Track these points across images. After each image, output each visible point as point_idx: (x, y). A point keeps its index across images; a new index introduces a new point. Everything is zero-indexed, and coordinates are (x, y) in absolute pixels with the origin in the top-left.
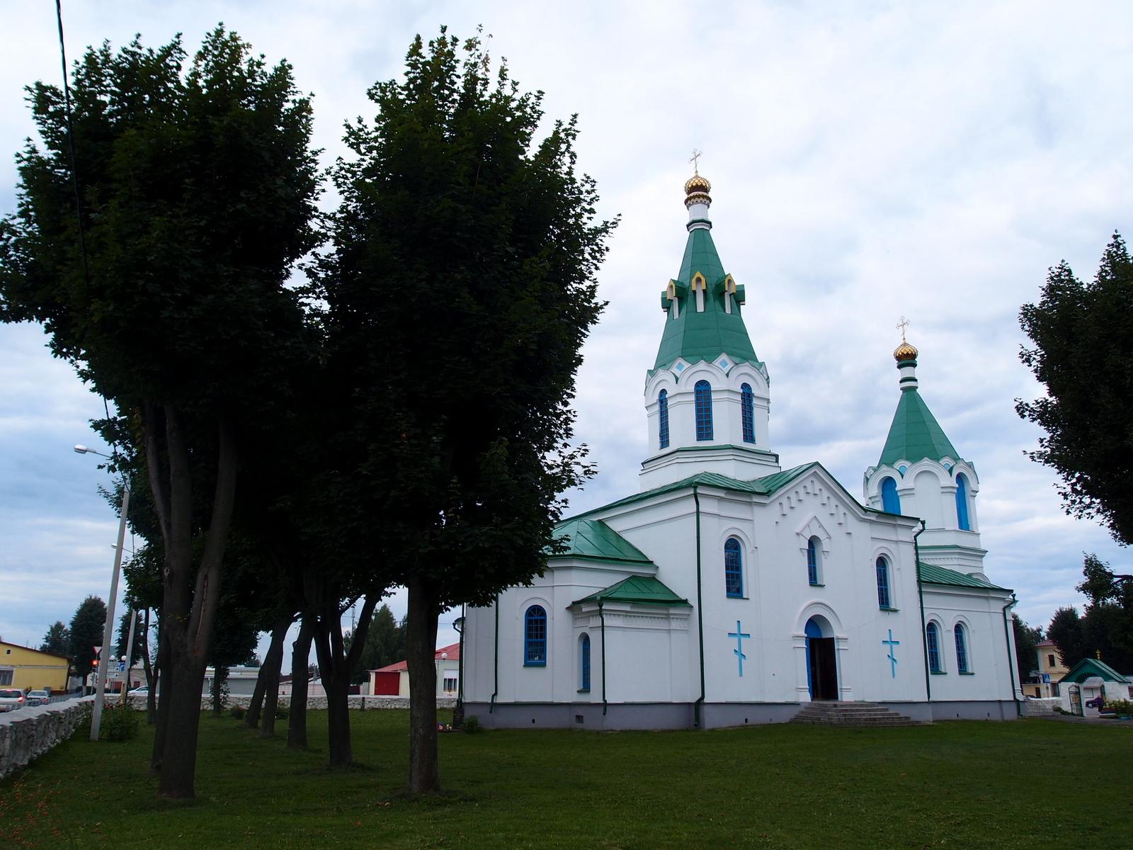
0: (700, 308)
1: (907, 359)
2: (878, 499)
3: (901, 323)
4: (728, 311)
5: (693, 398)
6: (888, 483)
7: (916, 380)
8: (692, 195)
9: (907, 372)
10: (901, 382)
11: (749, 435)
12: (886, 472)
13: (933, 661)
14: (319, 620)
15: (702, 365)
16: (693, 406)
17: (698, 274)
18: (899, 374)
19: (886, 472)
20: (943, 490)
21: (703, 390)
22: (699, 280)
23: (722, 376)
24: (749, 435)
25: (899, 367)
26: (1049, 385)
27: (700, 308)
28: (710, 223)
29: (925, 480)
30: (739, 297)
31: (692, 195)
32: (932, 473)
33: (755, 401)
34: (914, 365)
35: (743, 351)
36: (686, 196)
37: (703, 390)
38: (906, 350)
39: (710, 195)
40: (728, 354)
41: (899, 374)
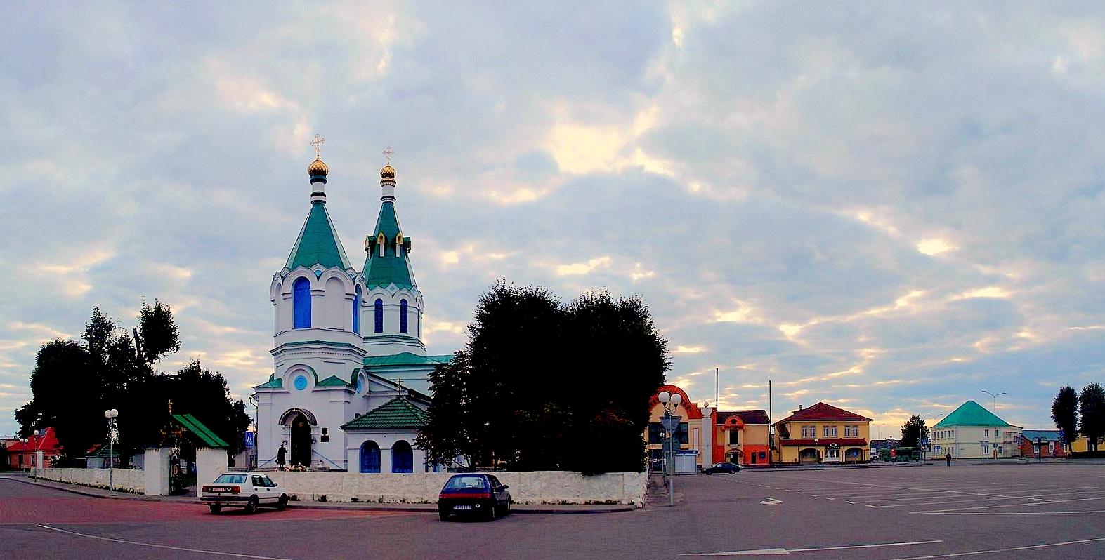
0: (382, 255)
1: (318, 175)
2: (290, 296)
3: (315, 140)
4: (398, 255)
5: (374, 308)
6: (301, 283)
7: (325, 196)
8: (385, 179)
9: (318, 186)
10: (312, 195)
11: (404, 328)
12: (301, 272)
13: (952, 506)
14: (111, 413)
15: (378, 290)
16: (374, 313)
17: (381, 234)
18: (311, 188)
19: (301, 272)
20: (347, 297)
21: (379, 305)
22: (381, 237)
23: (390, 296)
24: (404, 328)
25: (312, 182)
26: (571, 315)
27: (382, 255)
28: (393, 197)
29: (334, 284)
30: (406, 246)
31: (385, 179)
32: (337, 278)
33: (408, 309)
34: (325, 182)
35: (404, 280)
36: (381, 179)
37: (379, 305)
38: (317, 166)
39: (395, 179)
40: (395, 283)
41: (311, 188)
